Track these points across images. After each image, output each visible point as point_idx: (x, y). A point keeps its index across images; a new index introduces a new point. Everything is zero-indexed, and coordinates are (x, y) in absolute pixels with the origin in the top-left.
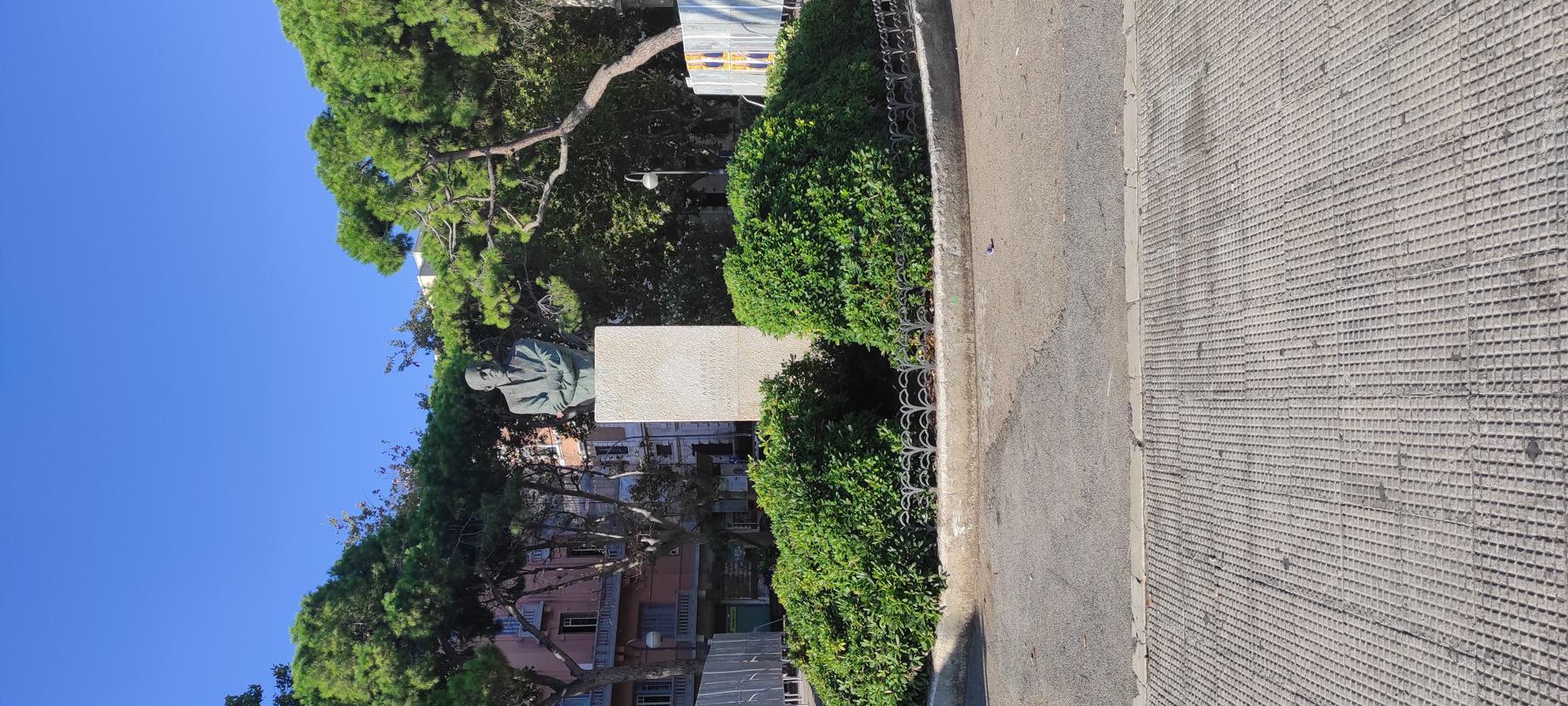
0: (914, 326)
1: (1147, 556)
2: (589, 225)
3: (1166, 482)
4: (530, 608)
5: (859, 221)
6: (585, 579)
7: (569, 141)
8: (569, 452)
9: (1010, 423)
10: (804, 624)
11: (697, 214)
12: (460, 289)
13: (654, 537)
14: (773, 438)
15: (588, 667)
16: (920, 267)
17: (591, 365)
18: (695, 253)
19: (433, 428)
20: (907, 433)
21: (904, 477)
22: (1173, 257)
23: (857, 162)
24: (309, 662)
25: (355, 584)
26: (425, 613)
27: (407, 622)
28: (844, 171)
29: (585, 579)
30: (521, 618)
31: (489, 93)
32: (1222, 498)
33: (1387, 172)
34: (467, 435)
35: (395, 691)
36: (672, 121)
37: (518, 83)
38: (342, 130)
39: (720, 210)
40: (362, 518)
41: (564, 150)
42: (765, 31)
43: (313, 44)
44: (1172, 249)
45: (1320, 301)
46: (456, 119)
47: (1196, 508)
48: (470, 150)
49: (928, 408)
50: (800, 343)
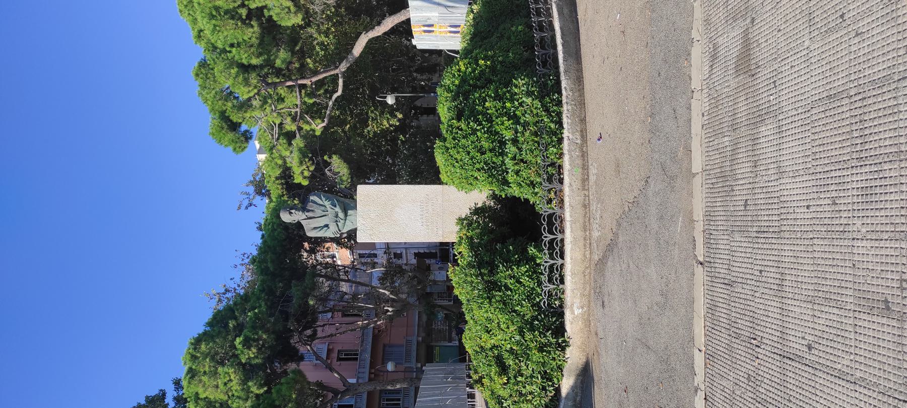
0: (551, 186)
1: (705, 335)
2: (355, 126)
3: (720, 289)
4: (320, 346)
5: (517, 122)
6: (352, 330)
7: (344, 77)
8: (343, 257)
9: (611, 247)
10: (482, 366)
11: (417, 119)
12: (280, 162)
13: (392, 307)
14: (464, 252)
15: (353, 381)
16: (555, 150)
17: (355, 208)
18: (417, 142)
19: (264, 242)
20: (546, 252)
21: (544, 278)
22: (727, 144)
23: (516, 86)
24: (192, 377)
25: (220, 332)
26: (259, 349)
27: (249, 355)
28: (508, 92)
29: (352, 330)
30: (315, 353)
31: (297, 48)
32: (761, 301)
33: (893, 86)
34: (283, 250)
35: (242, 394)
36: (404, 65)
37: (315, 42)
38: (212, 69)
39: (431, 117)
40: (224, 294)
41: (341, 82)
42: (459, 11)
43: (196, 19)
44: (726, 139)
45: (838, 173)
46: (278, 63)
47: (742, 306)
48: (286, 81)
49: (560, 237)
50: (480, 196)
